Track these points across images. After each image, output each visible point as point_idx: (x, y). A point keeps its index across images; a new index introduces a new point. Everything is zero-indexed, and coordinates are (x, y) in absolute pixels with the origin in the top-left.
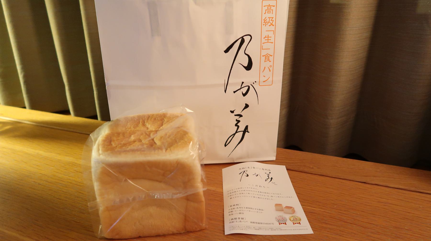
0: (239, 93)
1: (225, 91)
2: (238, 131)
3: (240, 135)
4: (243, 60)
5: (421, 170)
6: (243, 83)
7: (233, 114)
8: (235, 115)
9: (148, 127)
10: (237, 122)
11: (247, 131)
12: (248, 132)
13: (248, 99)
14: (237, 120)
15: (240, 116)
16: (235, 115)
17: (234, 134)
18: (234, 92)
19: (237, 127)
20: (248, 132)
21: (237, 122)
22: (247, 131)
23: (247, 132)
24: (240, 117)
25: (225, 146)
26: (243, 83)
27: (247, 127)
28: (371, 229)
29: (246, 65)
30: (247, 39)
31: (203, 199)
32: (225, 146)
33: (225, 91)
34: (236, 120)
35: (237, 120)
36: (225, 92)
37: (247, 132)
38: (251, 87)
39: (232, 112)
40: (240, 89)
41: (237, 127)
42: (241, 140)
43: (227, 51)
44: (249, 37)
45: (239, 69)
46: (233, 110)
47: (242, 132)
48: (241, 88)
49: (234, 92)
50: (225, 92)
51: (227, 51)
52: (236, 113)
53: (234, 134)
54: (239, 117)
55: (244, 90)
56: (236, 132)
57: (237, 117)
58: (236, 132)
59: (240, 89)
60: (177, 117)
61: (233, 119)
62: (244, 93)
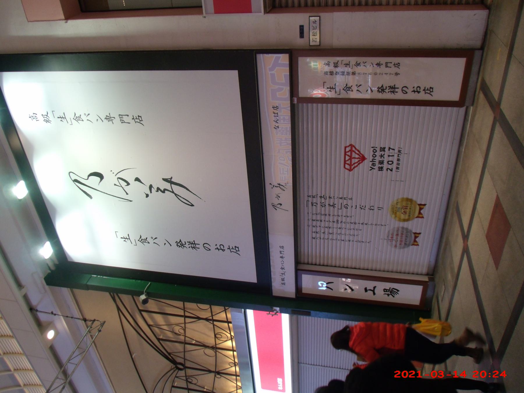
1: (131, 201)
3: (176, 188)
4: (279, 206)
6: (115, 185)
8: (151, 192)
9: (10, 335)
10: (159, 191)
11: (170, 180)
12: (172, 178)
13: (131, 180)
14: (157, 191)
15: (151, 187)
16: (151, 192)
17: (176, 195)
19: (166, 191)
20: (172, 178)
21: (159, 191)
22: (170, 180)
23: (172, 180)
24: (153, 187)
26: (115, 185)
27: (165, 180)
28: (373, 221)
29: (280, 205)
33: (131, 201)
34: (156, 191)
35: (157, 191)
36: (132, 201)
37: (172, 180)
40: (123, 188)
41: (166, 191)
42: (182, 187)
43: (276, 210)
45: (281, 207)
46: (146, 195)
48: (122, 187)
50: (132, 201)
51: (276, 210)
53: (176, 195)
54: (152, 188)
56: (173, 192)
57: (274, 187)
58: (173, 192)
59: (123, 188)
60: (498, 198)
62: (126, 184)
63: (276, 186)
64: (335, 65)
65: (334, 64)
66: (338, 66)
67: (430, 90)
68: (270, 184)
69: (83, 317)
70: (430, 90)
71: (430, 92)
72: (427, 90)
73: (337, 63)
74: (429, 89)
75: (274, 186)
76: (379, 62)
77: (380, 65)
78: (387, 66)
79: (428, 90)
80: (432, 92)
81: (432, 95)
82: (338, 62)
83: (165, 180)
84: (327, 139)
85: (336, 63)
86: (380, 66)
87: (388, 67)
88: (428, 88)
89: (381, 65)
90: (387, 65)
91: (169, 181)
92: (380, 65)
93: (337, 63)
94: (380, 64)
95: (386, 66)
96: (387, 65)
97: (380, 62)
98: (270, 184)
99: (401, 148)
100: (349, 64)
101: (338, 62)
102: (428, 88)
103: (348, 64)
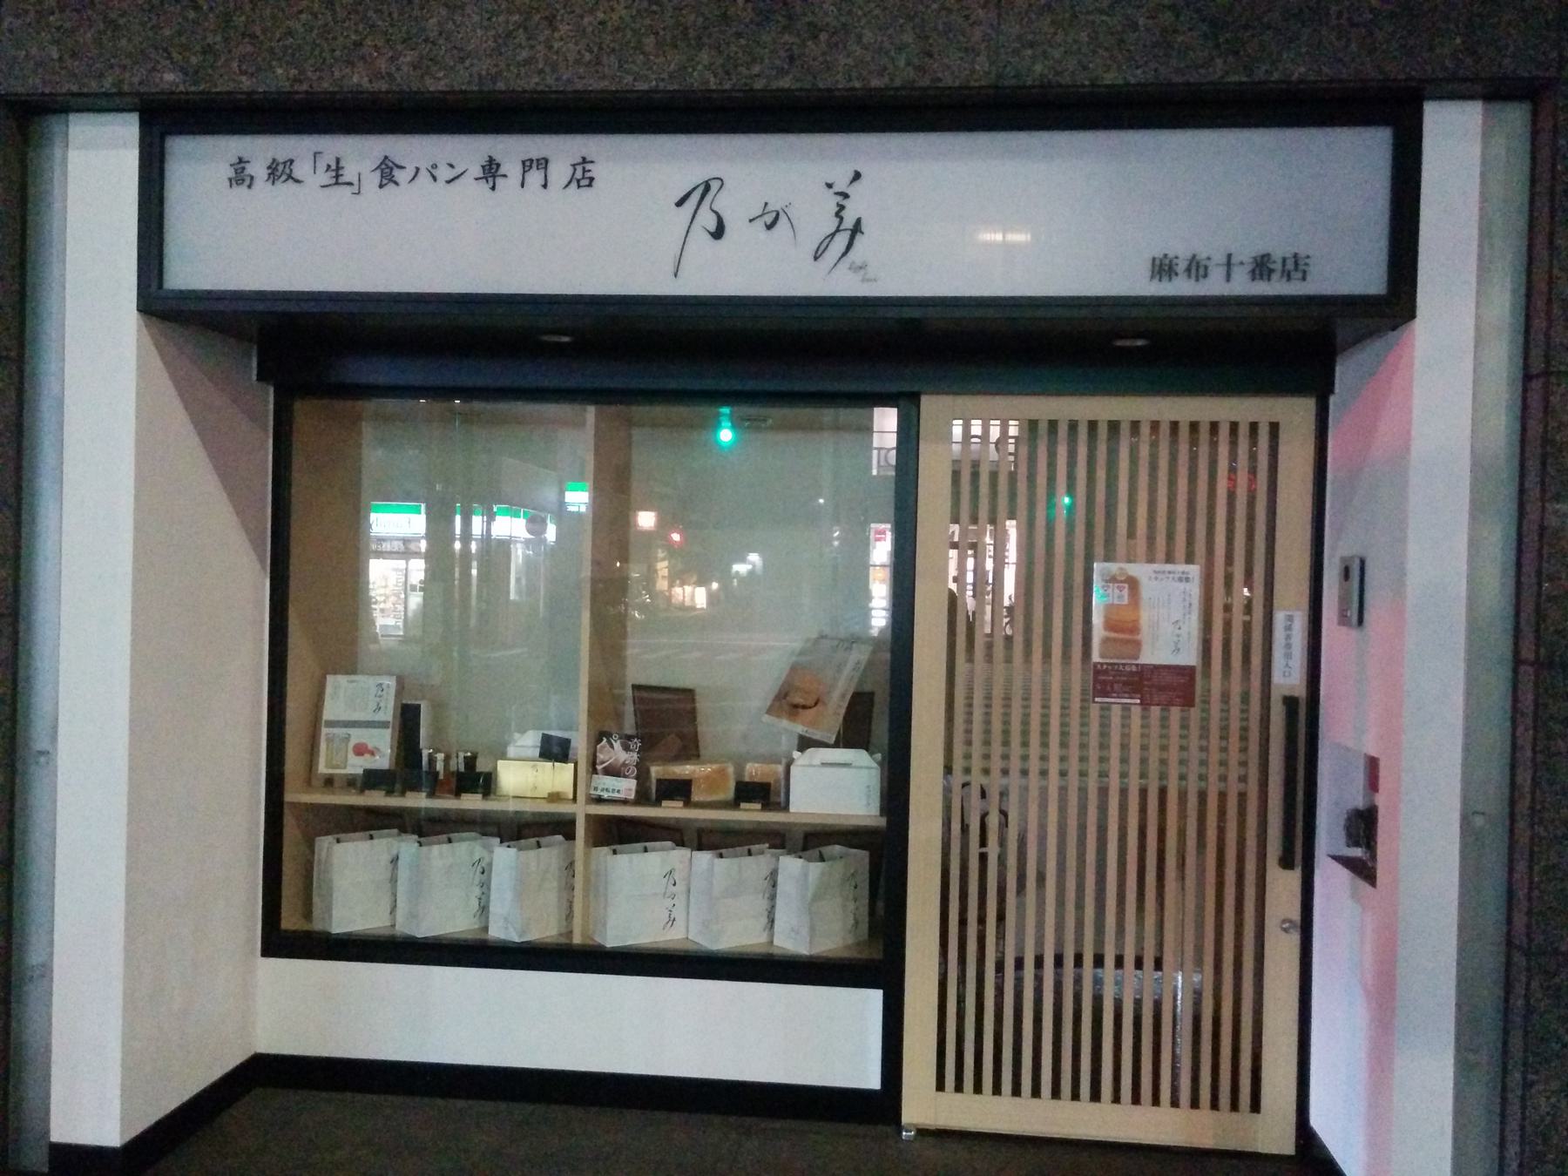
0: (760, 224)
1: (676, 276)
2: (841, 228)
3: (841, 241)
4: (707, 220)
5: (1386, 278)
6: (766, 204)
7: (832, 191)
8: (837, 194)
14: (838, 205)
16: (837, 194)
17: (833, 235)
18: (751, 221)
25: (816, 258)
27: (858, 221)
30: (715, 185)
31: (457, 556)
32: (816, 258)
38: (781, 213)
39: (830, 186)
43: (680, 203)
44: (720, 182)
45: (700, 238)
47: (849, 232)
49: (751, 221)
51: (680, 203)
52: (837, 189)
55: (769, 219)
57: (839, 199)
58: (838, 230)
61: (831, 203)
63: (842, 208)
64: (280, 168)
65: (285, 163)
66: (278, 183)
67: (583, 178)
68: (857, 176)
69: (430, 768)
70: (583, 178)
71: (578, 181)
72: (584, 168)
73: (290, 177)
74: (588, 175)
75: (846, 196)
76: (502, 171)
77: (490, 180)
78: (531, 167)
79: (584, 171)
80: (579, 186)
81: (567, 186)
82: (297, 181)
83: (858, 221)
84: (1082, 828)
85: (291, 170)
86: (486, 178)
87: (524, 172)
88: (589, 171)
89: (491, 184)
90: (534, 165)
91: (857, 229)
92: (490, 180)
93: (290, 177)
94: (494, 177)
95: (531, 160)
96: (534, 165)
97: (505, 176)
98: (857, 176)
99: (1152, 654)
100: (337, 183)
101: (297, 181)
102: (589, 171)
103: (341, 180)
